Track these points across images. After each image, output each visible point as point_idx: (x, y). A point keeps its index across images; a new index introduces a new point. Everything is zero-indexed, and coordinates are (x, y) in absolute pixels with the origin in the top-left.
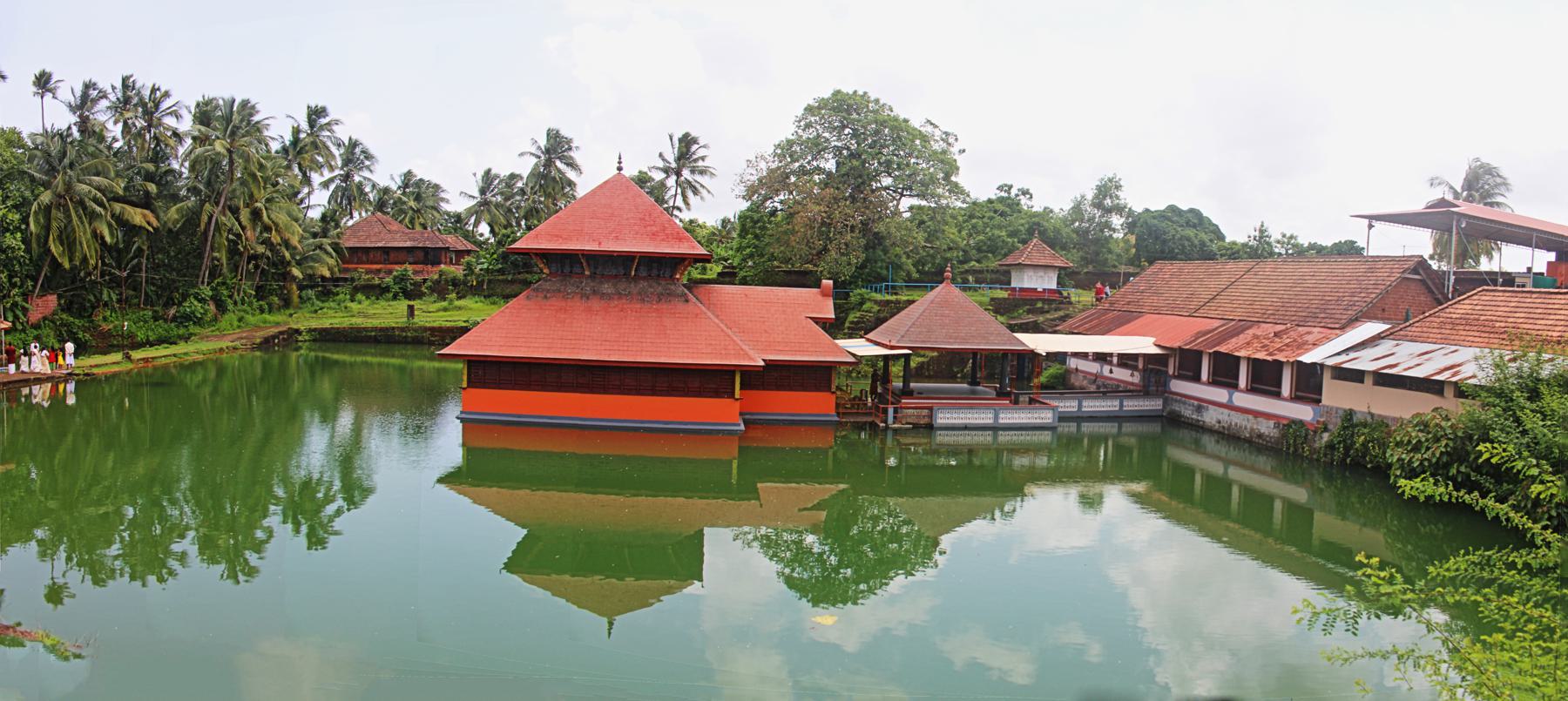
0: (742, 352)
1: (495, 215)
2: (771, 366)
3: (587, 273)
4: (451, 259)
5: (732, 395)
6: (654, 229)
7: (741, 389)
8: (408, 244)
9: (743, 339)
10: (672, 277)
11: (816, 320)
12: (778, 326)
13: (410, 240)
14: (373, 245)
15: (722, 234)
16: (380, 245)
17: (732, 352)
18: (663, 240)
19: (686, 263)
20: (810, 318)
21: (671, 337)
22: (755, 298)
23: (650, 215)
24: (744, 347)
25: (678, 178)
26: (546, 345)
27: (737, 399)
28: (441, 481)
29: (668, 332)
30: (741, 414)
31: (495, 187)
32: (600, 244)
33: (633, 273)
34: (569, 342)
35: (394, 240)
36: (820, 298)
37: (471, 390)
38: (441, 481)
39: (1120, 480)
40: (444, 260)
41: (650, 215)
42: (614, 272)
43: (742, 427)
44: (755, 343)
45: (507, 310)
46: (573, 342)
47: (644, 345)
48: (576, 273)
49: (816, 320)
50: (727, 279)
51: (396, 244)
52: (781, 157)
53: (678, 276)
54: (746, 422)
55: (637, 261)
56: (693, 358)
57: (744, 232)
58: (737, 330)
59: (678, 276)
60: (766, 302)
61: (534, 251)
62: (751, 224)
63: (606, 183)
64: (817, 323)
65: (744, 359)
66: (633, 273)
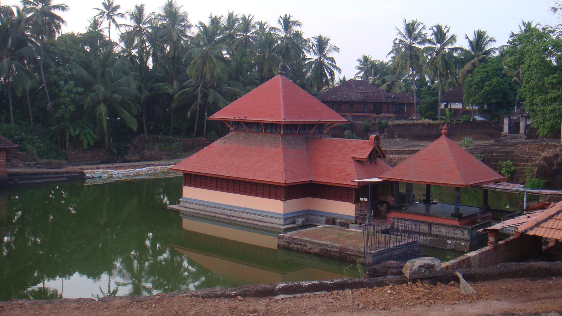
33: (263, 131)
66: (263, 131)
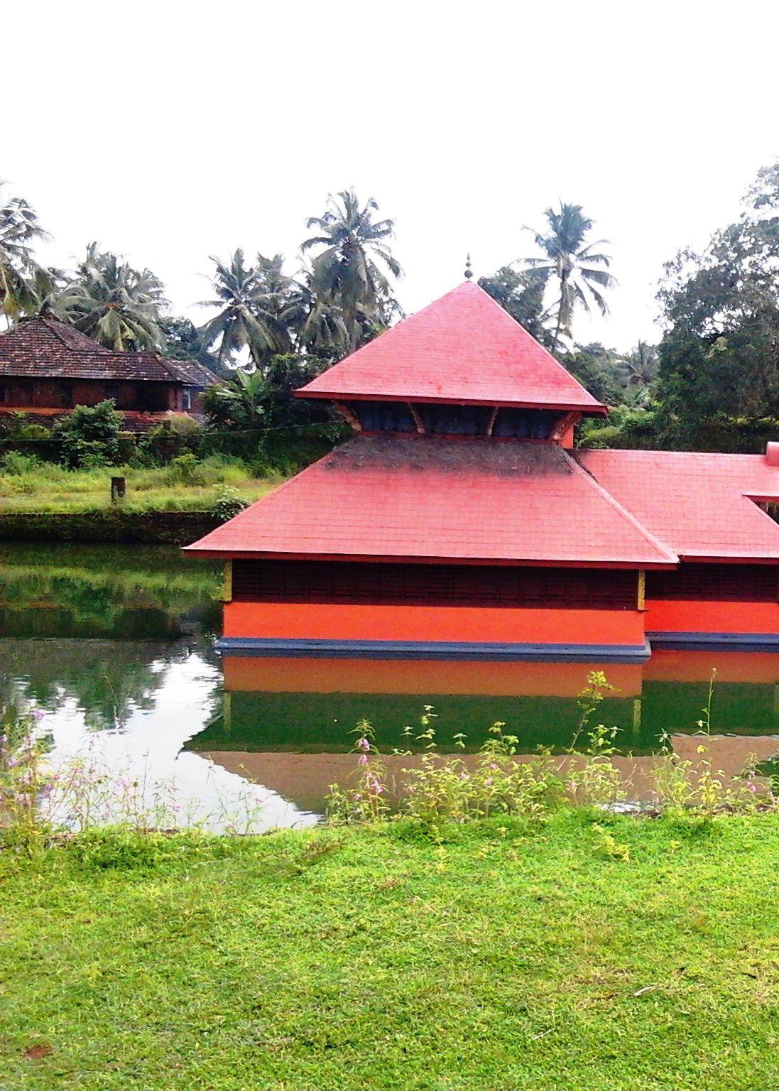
0: (646, 545)
1: (256, 331)
2: (687, 564)
3: (420, 430)
4: (185, 403)
5: (632, 605)
6: (521, 367)
7: (645, 598)
8: (107, 374)
9: (650, 526)
10: (547, 438)
11: (759, 501)
12: (702, 509)
13: (111, 368)
14: (40, 374)
15: (635, 368)
16: (54, 373)
17: (634, 545)
18: (535, 384)
19: (569, 417)
20: (749, 497)
21: (546, 523)
22: (669, 469)
23: (515, 346)
24: (651, 537)
25: (563, 279)
26: (359, 536)
27: (641, 612)
28: (187, 747)
29: (542, 516)
30: (646, 634)
31: (251, 281)
32: (440, 388)
33: (490, 432)
34: (392, 531)
35: (79, 366)
36: (764, 468)
37: (238, 604)
38: (187, 747)
39: (23, 407)
40: (172, 404)
41: (515, 346)
42: (461, 430)
43: (648, 651)
44: (668, 533)
45: (295, 484)
46: (399, 531)
47: (505, 535)
48: (403, 431)
49: (759, 501)
50: (643, 440)
51: (84, 374)
52: (720, 252)
53: (556, 437)
54: (654, 645)
55: (495, 414)
56: (577, 553)
57: (667, 366)
58: (642, 514)
59: (556, 437)
60: (321, 525)
61: (338, 397)
62: (550, 430)
63: (448, 295)
64: (758, 504)
65: (650, 555)
